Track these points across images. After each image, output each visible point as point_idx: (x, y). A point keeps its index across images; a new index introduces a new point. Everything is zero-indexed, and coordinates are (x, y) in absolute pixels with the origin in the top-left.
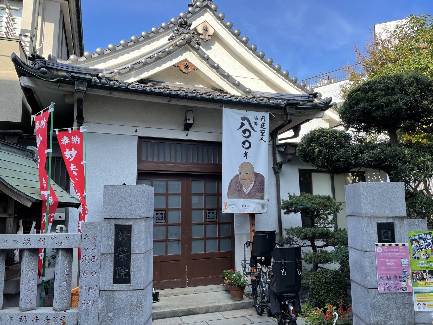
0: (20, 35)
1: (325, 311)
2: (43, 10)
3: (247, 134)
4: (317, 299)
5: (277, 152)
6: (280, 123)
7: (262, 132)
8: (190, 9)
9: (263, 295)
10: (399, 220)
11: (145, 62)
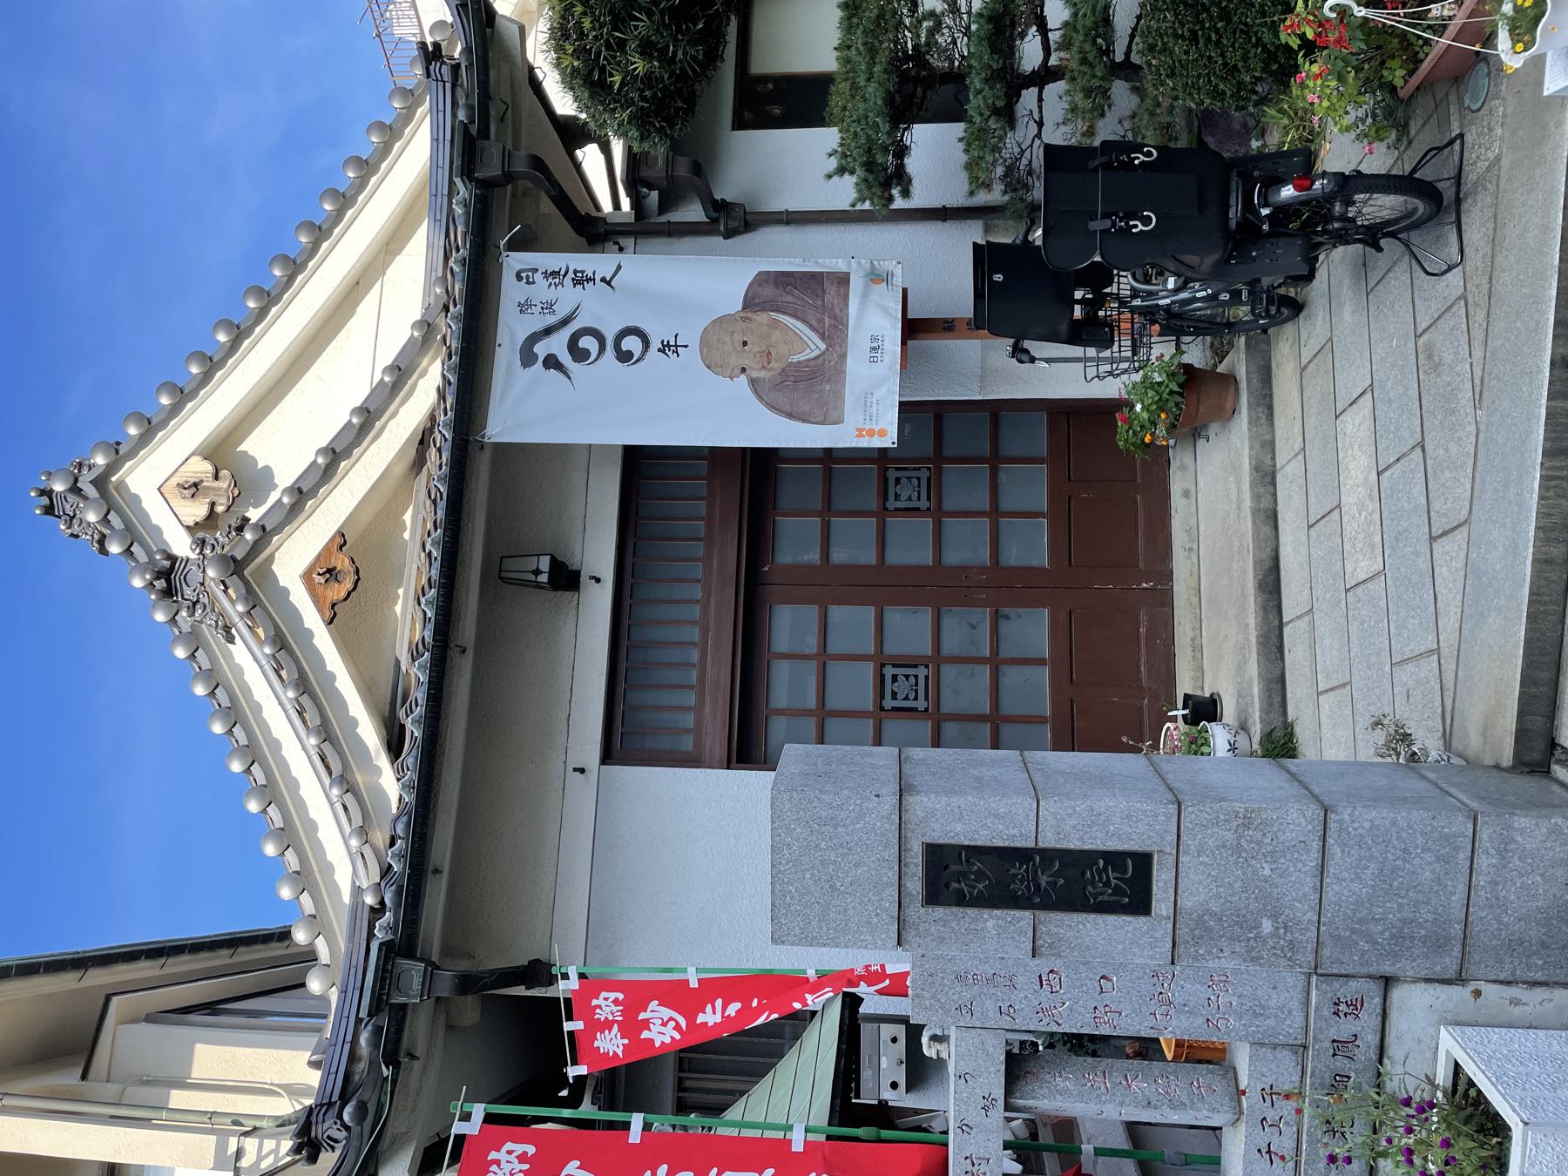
1: (1309, 47)
2: (147, 1083)
3: (587, 343)
4: (1258, 79)
5: (663, 219)
6: (547, 206)
7: (581, 280)
8: (115, 548)
9: (1225, 296)
11: (318, 733)
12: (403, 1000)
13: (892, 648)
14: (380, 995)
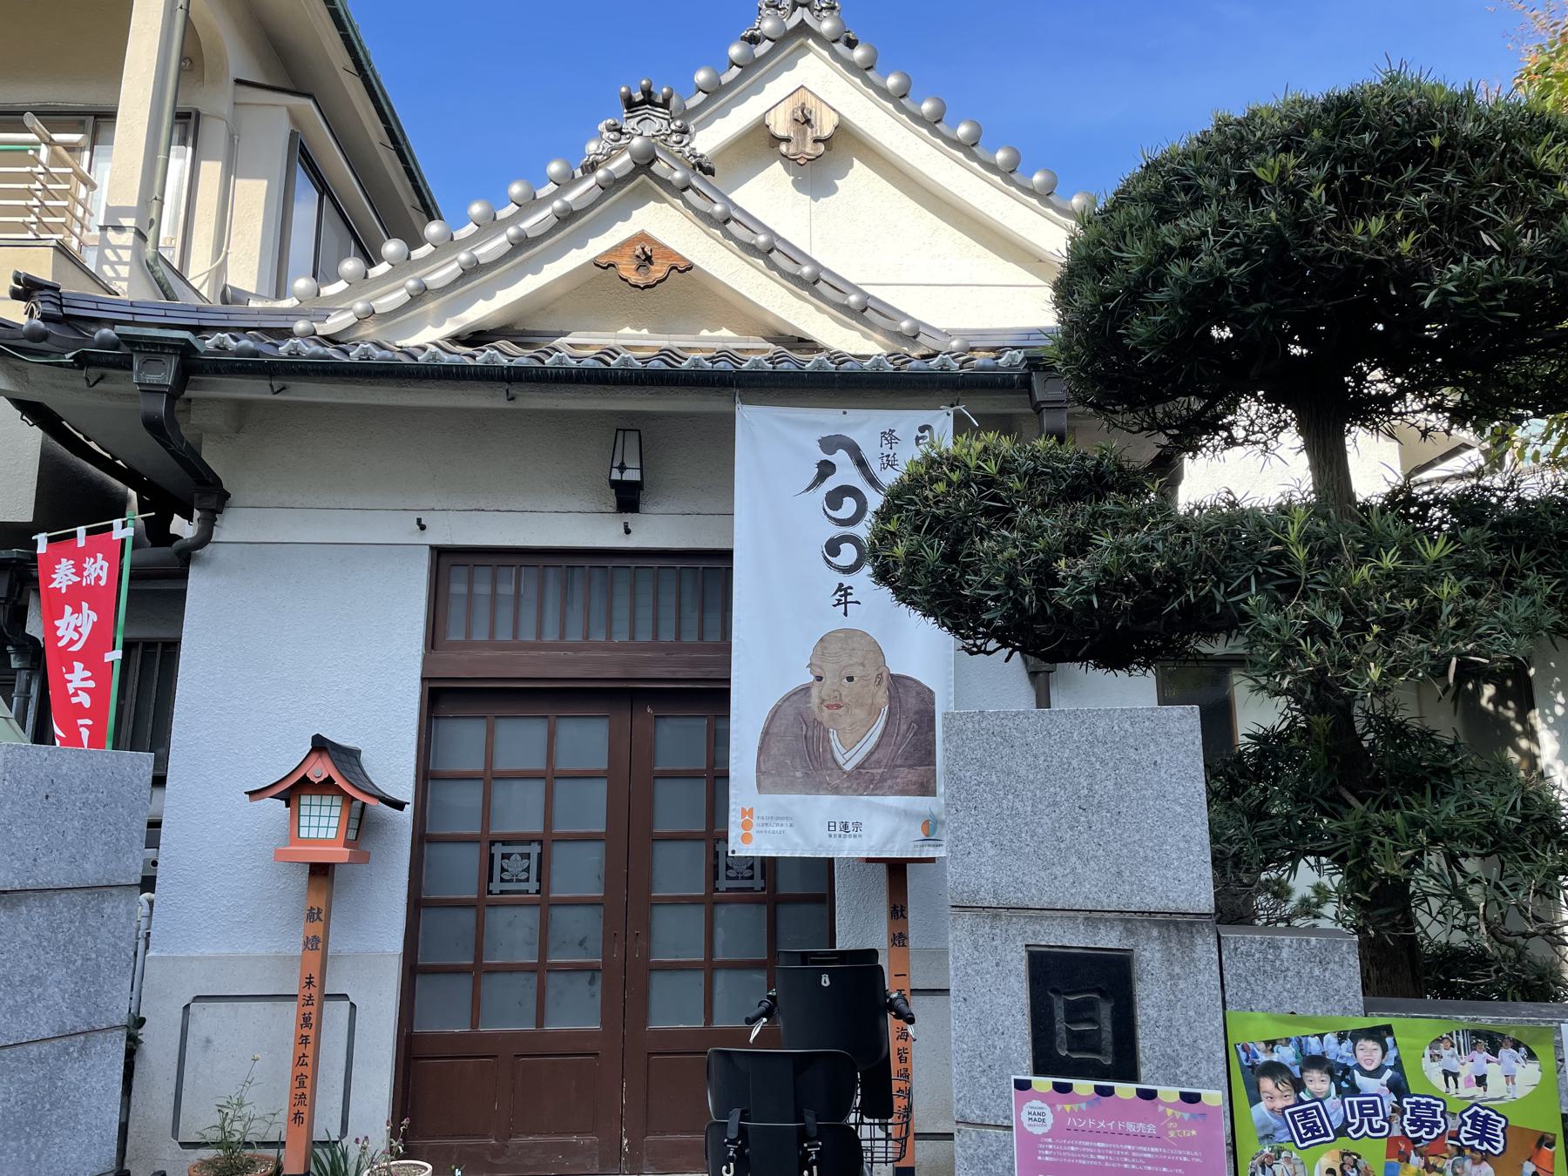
0: (103, 228)
3: (849, 507)
10: (1165, 941)
12: (136, 367)
13: (560, 853)
14: (139, 344)
